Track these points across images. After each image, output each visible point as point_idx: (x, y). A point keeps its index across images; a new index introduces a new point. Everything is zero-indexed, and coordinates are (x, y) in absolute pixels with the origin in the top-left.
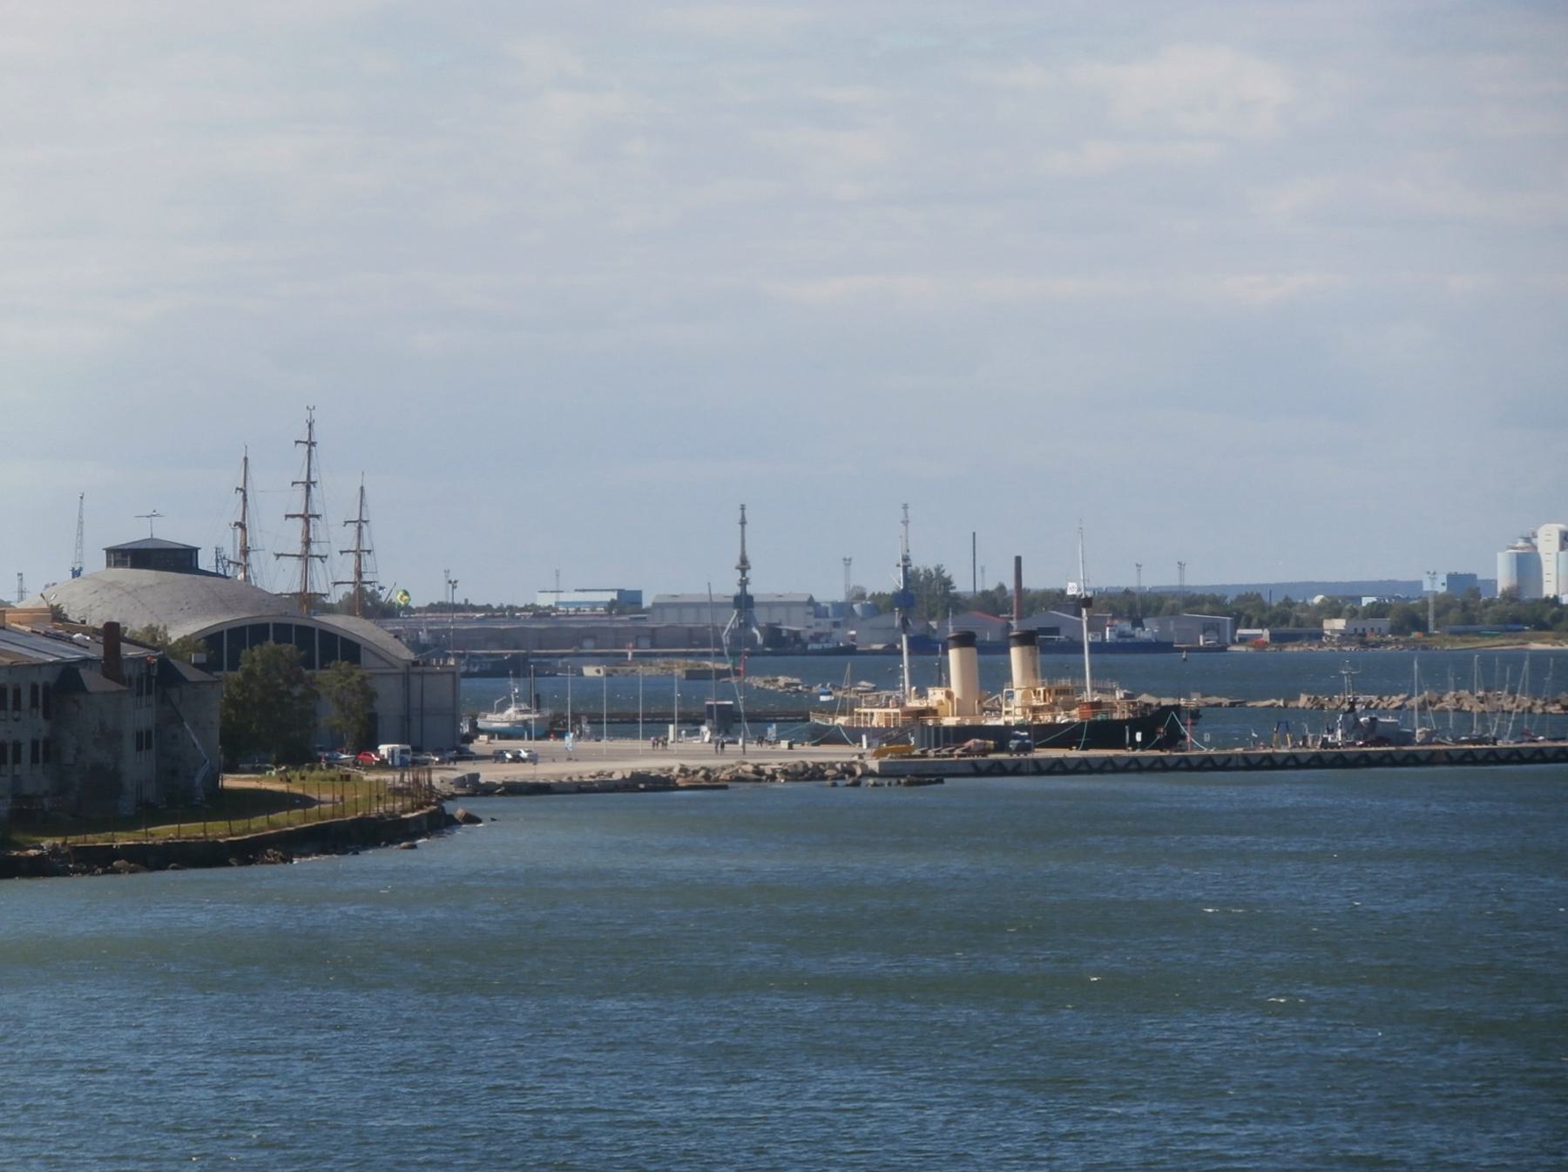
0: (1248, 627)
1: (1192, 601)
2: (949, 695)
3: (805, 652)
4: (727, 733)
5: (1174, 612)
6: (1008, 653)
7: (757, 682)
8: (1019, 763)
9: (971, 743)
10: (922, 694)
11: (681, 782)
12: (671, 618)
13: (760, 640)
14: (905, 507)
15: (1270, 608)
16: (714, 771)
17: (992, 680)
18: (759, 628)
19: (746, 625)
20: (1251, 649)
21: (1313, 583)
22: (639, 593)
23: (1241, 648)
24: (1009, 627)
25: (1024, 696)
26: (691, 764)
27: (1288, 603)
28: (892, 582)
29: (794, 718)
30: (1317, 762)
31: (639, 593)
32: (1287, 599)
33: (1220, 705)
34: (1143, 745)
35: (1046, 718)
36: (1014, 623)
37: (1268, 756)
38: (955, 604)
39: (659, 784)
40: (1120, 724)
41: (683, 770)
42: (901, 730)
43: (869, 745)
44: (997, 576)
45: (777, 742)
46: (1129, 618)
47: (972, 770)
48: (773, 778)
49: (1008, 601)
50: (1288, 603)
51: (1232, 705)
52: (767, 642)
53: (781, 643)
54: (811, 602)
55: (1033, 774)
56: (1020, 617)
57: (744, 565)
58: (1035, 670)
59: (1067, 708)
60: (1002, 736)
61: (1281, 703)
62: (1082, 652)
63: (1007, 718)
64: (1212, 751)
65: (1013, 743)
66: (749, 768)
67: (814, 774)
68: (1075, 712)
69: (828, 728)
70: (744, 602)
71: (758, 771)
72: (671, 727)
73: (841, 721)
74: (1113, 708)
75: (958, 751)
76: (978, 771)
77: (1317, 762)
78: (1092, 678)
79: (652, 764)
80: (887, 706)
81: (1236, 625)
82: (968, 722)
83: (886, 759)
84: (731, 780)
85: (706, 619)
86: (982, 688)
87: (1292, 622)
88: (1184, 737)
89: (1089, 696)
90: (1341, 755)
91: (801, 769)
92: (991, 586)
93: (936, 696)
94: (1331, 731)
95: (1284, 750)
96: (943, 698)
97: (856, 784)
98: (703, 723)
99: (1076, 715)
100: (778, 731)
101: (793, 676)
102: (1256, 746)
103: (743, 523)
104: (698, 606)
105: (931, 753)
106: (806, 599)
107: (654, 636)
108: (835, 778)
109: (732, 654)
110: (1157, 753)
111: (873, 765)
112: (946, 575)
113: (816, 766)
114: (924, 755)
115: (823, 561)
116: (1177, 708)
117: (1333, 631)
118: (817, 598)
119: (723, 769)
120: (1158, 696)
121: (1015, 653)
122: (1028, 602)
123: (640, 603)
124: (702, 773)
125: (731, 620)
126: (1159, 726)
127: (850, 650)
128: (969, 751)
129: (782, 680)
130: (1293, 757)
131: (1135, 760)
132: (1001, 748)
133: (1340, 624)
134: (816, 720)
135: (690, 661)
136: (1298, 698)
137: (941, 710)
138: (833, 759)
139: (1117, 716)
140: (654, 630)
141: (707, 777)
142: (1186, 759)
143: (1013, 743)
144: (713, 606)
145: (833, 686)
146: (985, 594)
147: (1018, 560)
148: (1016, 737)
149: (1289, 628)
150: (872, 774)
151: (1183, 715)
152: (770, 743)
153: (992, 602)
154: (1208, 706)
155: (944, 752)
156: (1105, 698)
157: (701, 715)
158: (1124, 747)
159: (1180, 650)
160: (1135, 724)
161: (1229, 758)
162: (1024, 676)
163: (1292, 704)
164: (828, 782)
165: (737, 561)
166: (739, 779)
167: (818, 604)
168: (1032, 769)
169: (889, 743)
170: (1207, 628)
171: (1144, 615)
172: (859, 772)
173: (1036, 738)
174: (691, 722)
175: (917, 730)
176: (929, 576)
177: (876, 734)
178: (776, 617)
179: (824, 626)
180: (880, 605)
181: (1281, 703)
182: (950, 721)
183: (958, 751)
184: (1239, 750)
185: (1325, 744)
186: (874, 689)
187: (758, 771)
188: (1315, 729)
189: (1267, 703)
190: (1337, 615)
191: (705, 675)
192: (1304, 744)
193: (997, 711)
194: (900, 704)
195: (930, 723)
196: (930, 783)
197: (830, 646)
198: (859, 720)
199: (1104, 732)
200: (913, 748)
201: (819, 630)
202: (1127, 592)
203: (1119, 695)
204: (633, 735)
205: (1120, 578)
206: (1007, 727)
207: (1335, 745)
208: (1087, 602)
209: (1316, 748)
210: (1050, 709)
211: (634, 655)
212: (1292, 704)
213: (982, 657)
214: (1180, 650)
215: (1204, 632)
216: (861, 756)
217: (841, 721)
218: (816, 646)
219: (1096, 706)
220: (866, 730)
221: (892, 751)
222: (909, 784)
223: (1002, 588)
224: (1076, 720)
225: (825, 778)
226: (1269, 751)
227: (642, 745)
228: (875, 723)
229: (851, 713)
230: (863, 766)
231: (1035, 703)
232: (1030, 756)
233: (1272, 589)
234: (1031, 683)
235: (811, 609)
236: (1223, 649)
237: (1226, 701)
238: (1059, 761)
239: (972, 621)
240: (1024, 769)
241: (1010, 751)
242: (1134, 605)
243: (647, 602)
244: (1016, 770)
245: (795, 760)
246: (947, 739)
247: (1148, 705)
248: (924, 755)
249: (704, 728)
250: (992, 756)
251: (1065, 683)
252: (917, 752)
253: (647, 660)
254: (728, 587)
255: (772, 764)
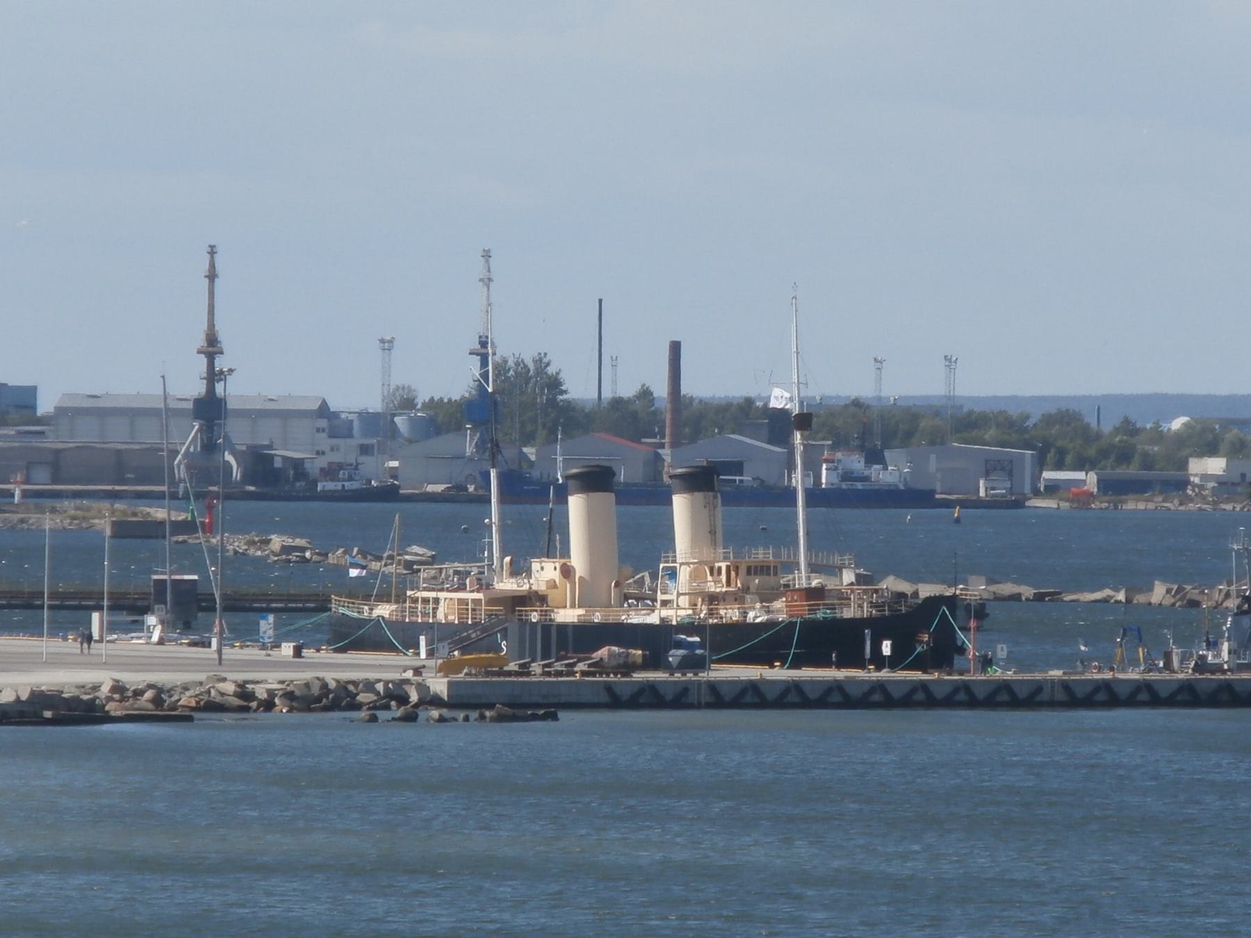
0: (1059, 466)
1: (966, 423)
2: (567, 572)
3: (312, 495)
4: (187, 627)
5: (936, 439)
6: (670, 503)
7: (237, 544)
8: (685, 689)
9: (603, 653)
10: (520, 569)
11: (113, 708)
12: (86, 434)
13: (236, 473)
14: (487, 255)
15: (1099, 436)
16: (170, 691)
17: (641, 550)
18: (234, 453)
19: (210, 447)
20: (1065, 505)
21: (1165, 397)
22: (32, 391)
23: (1050, 503)
24: (658, 458)
25: (694, 576)
26: (133, 679)
27: (1128, 428)
28: (454, 380)
29: (303, 606)
30: (1187, 696)
31: (32, 391)
32: (1127, 421)
33: (1016, 597)
34: (894, 662)
35: (730, 614)
36: (666, 453)
37: (1106, 685)
38: (564, 419)
39: (78, 711)
40: (855, 626)
41: (118, 688)
42: (484, 629)
43: (431, 654)
44: (638, 373)
45: (277, 645)
46: (862, 448)
47: (604, 698)
48: (268, 705)
49: (655, 417)
50: (1128, 428)
51: (1039, 597)
52: (248, 477)
53: (271, 479)
54: (324, 411)
55: (709, 706)
56: (675, 444)
57: (212, 347)
58: (713, 532)
59: (767, 597)
60: (656, 641)
61: (1121, 596)
62: (794, 503)
63: (665, 613)
64: (1010, 675)
65: (675, 656)
66: (230, 688)
67: (339, 699)
68: (779, 604)
69: (362, 623)
70: (210, 409)
71: (244, 694)
72: (95, 616)
73: (384, 610)
74: (843, 598)
75: (581, 666)
76: (615, 701)
77: (1187, 696)
78: (809, 547)
79: (65, 678)
80: (462, 588)
81: (1041, 464)
82: (597, 618)
83: (460, 677)
84: (197, 709)
85: (148, 435)
86: (624, 557)
87: (1137, 459)
88: (962, 650)
89: (802, 578)
90: (1228, 686)
91: (316, 691)
92: (627, 390)
93: (544, 573)
94: (1213, 645)
95: (1133, 675)
96: (556, 575)
97: (410, 718)
98: (146, 610)
99: (781, 610)
100: (277, 626)
101: (295, 535)
102: (1086, 667)
103: (212, 276)
104: (133, 414)
105: (536, 668)
106: (315, 406)
107: (57, 464)
108: (374, 707)
109: (198, 496)
110: (917, 675)
111: (439, 685)
112: (551, 370)
113: (343, 686)
114: (524, 670)
115: (341, 348)
116: (952, 601)
117: (1205, 477)
118: (334, 406)
119: (186, 688)
120: (915, 578)
121: (680, 504)
122: (692, 419)
123: (33, 407)
124: (149, 694)
125: (189, 438)
126: (922, 631)
127: (389, 494)
128: (599, 667)
129: (277, 542)
130: (1147, 686)
131: (880, 686)
132: (654, 661)
133: (1216, 465)
134: (342, 608)
135: (118, 506)
136: (1151, 589)
137: (553, 596)
138: (372, 676)
139: (848, 613)
140: (57, 452)
141: (157, 701)
142: (966, 687)
143: (675, 656)
144: (164, 414)
145: (363, 553)
146: (617, 403)
147: (675, 348)
148: (680, 644)
149: (1131, 471)
150: (436, 701)
151: (960, 613)
152: (264, 647)
153: (631, 418)
154: (998, 598)
155: (558, 666)
156: (831, 584)
157: (145, 596)
158: (862, 666)
159: (948, 504)
160: (881, 627)
161: (1039, 687)
162: (695, 540)
163: (1140, 599)
164: (363, 714)
165: (201, 341)
166: (213, 707)
167: (336, 415)
168: (705, 698)
169: (464, 651)
170: (991, 468)
171: (887, 445)
172: (414, 697)
173: (715, 649)
174: (129, 609)
175: (513, 628)
176: (523, 373)
177: (442, 634)
178: (265, 434)
179: (345, 452)
180: (442, 419)
181: (1121, 596)
182: (568, 615)
183: (581, 666)
184: (1056, 673)
185: (1201, 666)
186: (433, 560)
187: (244, 694)
188: (1185, 641)
189: (1098, 595)
190: (1211, 450)
191: (153, 530)
192: (1168, 666)
193: (646, 600)
194: (483, 585)
195: (535, 617)
196: (535, 717)
197: (354, 485)
198: (413, 613)
199: (826, 639)
200: (506, 661)
201: (337, 458)
202: (857, 403)
203: (848, 577)
204: (33, 629)
205: (845, 380)
206: (665, 626)
207: (1218, 669)
208: (804, 421)
209: (1184, 673)
210: (738, 598)
211: (25, 494)
212: (1140, 599)
213: (622, 508)
214: (948, 504)
215: (987, 474)
216: (417, 671)
217: (384, 610)
218: (331, 486)
219: (815, 594)
220: (428, 628)
221: (470, 663)
222: (500, 718)
223: (646, 394)
224: (781, 617)
225: (357, 707)
226: (1108, 675)
227: (46, 645)
228: (440, 616)
229: (400, 598)
230: (422, 688)
231: (712, 587)
232: (703, 676)
233: (1101, 404)
234: (707, 554)
235: (323, 423)
236: (1018, 504)
237: (1027, 591)
238: (753, 687)
239: (601, 447)
240: (692, 698)
241: (669, 668)
242: (869, 428)
243: (45, 406)
244: (680, 699)
245: (307, 675)
246: (562, 645)
247: (902, 595)
248: (524, 670)
249: (151, 620)
250: (639, 676)
251: (762, 555)
252: (512, 666)
253: (49, 503)
254: (189, 384)
255: (267, 682)
